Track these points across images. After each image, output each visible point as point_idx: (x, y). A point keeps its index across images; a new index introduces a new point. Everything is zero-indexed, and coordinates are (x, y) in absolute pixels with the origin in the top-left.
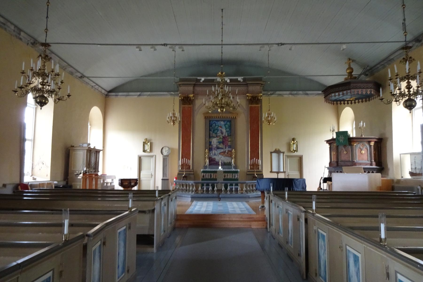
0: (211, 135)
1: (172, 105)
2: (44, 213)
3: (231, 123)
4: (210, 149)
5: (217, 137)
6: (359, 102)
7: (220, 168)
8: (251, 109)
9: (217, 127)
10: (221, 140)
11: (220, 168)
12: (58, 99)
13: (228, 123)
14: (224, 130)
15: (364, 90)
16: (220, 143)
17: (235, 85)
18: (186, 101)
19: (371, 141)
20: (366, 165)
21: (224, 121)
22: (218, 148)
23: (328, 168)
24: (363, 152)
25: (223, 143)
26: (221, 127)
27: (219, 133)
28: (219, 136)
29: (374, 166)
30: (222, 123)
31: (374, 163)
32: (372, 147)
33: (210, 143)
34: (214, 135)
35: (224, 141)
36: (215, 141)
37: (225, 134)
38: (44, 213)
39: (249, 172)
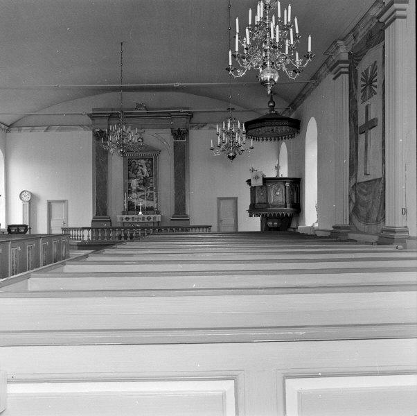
0: (130, 176)
1: (85, 139)
2: (157, 109)
3: (152, 163)
4: (130, 192)
5: (137, 177)
6: (271, 140)
7: (140, 213)
8: (176, 145)
9: (136, 166)
10: (142, 181)
11: (140, 213)
12: (273, 106)
13: (150, 162)
14: (145, 170)
15: (279, 127)
16: (140, 184)
17: (298, 252)
18: (100, 136)
19: (285, 182)
20: (280, 207)
21: (145, 159)
22: (138, 191)
23: (248, 211)
24: (278, 193)
25: (144, 184)
26: (141, 166)
27: (139, 174)
28: (140, 177)
29: (288, 208)
30: (143, 161)
31: (288, 205)
32: (288, 188)
33: (130, 184)
34: (134, 176)
35: (145, 182)
36: (134, 183)
37: (146, 174)
38: (157, 109)
39: (173, 217)
